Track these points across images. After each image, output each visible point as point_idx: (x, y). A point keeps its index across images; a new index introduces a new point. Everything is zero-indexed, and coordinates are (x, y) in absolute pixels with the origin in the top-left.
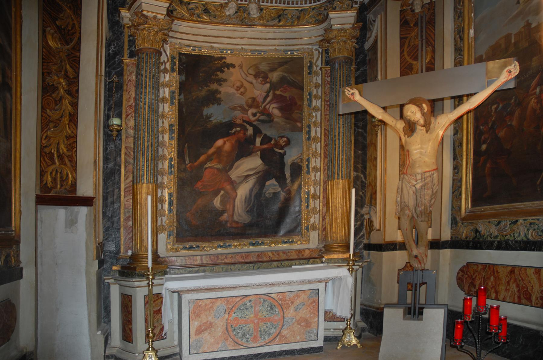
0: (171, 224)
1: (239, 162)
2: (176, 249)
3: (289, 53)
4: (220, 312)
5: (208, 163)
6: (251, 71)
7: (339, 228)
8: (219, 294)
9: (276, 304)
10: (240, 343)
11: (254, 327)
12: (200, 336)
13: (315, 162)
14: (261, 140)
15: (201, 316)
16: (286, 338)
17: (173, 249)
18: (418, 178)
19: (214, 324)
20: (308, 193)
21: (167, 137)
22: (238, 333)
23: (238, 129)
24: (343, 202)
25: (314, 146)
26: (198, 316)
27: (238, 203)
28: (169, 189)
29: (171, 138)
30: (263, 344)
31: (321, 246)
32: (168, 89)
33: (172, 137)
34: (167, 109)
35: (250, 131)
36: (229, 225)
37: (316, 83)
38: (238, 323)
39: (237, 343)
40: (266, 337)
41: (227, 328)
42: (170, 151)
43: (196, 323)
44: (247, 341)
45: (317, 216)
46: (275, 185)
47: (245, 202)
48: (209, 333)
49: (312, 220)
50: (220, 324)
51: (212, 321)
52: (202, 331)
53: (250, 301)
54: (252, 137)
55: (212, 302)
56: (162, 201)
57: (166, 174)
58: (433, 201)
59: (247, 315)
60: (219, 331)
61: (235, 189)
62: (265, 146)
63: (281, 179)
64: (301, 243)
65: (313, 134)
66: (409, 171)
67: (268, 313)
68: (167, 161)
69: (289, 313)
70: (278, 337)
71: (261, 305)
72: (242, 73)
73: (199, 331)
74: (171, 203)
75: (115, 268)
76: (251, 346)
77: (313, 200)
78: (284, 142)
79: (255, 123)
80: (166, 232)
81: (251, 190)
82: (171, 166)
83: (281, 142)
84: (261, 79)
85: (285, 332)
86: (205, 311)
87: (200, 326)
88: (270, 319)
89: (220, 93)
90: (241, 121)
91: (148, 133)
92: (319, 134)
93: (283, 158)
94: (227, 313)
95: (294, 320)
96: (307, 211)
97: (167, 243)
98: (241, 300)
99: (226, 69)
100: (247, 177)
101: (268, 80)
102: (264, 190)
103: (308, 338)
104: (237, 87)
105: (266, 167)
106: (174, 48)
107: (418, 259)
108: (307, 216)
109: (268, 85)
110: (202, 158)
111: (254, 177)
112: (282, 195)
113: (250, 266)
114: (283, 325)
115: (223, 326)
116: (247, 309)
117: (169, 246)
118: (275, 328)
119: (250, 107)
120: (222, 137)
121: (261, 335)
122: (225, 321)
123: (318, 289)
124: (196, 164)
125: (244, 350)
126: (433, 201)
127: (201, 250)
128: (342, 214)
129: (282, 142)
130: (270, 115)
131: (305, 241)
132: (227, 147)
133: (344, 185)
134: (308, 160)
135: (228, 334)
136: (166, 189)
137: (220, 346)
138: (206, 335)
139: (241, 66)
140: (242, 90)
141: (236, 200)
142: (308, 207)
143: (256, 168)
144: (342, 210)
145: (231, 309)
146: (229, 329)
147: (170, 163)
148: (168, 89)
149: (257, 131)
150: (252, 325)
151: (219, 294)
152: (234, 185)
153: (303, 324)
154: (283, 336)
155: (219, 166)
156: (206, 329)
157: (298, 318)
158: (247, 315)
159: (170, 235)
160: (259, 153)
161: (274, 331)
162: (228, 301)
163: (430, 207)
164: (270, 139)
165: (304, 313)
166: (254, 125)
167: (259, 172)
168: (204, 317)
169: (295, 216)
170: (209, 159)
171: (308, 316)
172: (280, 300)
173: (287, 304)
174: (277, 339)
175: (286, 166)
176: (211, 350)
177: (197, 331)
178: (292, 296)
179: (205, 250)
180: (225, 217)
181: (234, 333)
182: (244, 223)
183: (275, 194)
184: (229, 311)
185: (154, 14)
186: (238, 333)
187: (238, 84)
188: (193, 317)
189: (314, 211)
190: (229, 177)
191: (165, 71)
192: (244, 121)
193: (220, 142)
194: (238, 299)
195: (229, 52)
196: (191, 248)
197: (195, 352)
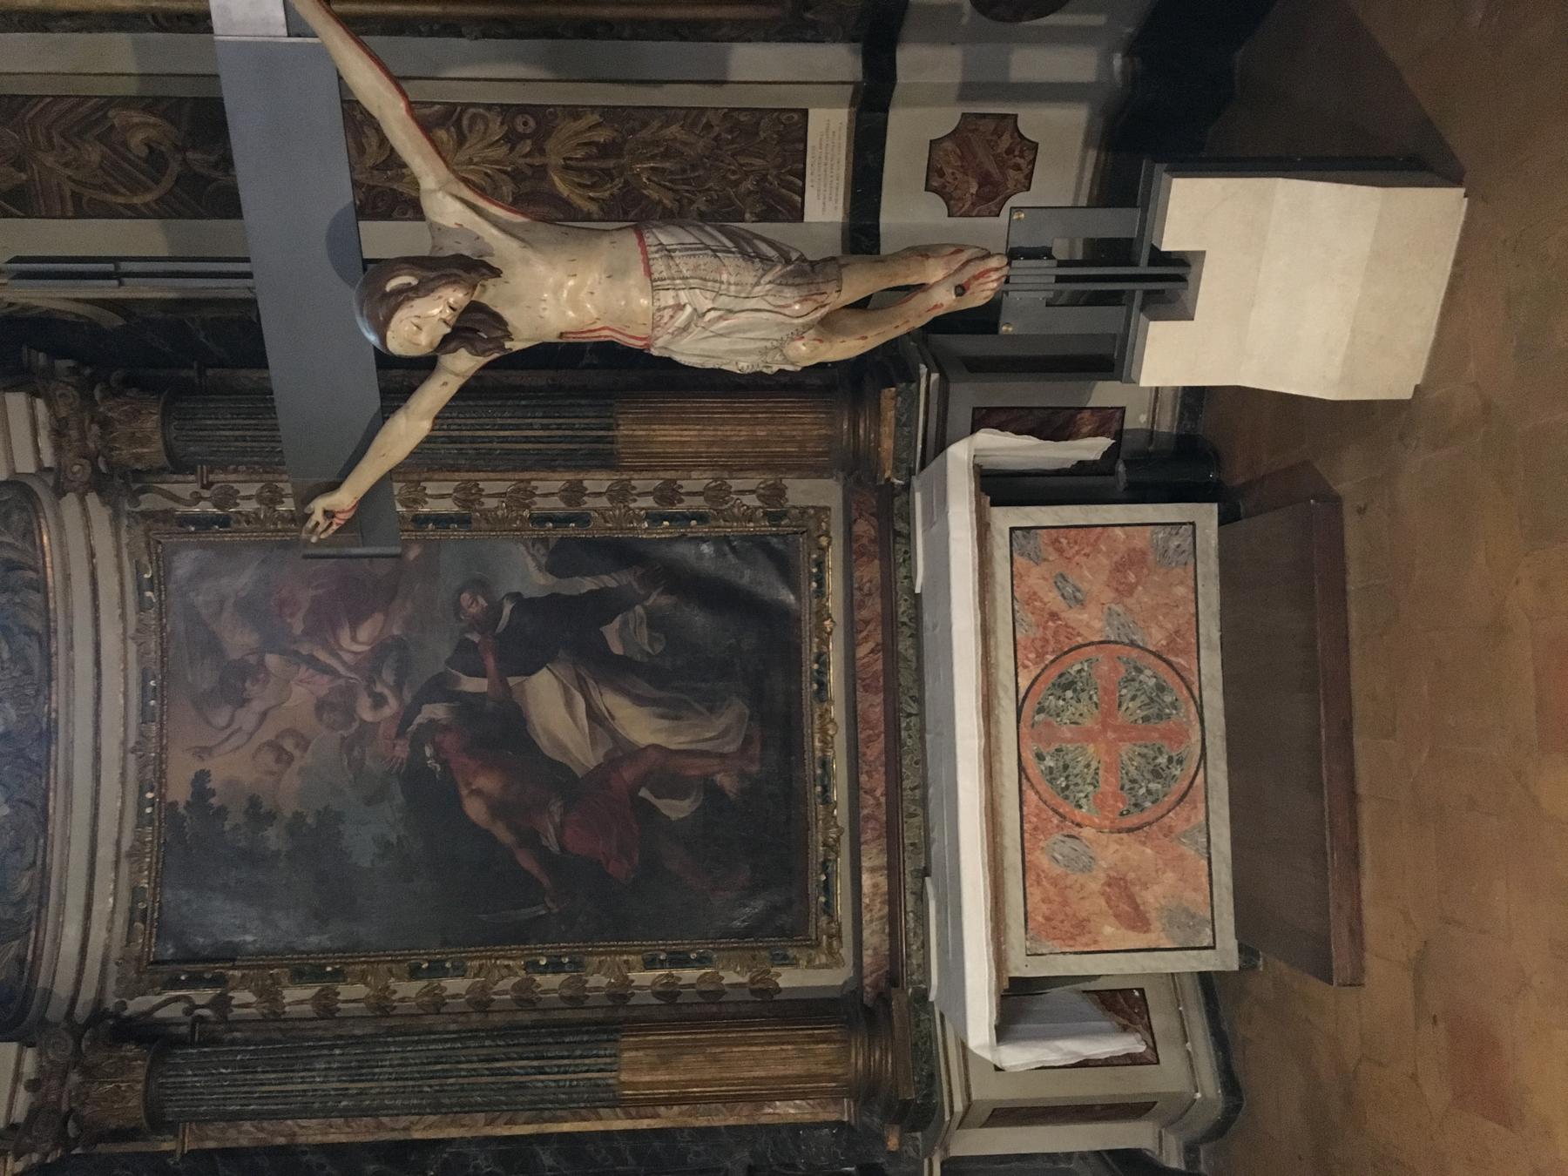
0: (748, 955)
1: (544, 743)
2: (830, 937)
3: (149, 594)
4: (1073, 855)
5: (544, 842)
6: (221, 718)
7: (787, 430)
8: (1012, 857)
9: (1053, 673)
10: (1186, 784)
11: (1130, 740)
12: (1152, 915)
13: (546, 495)
14: (470, 675)
15: (1084, 914)
16: (1177, 632)
17: (830, 945)
18: (671, 302)
19: (1113, 874)
20: (655, 518)
21: (455, 986)
22: (1149, 792)
23: (428, 751)
24: (698, 421)
25: (491, 503)
26: (1082, 925)
27: (682, 739)
28: (630, 970)
29: (460, 971)
30: (1193, 709)
31: (841, 475)
32: (285, 992)
33: (455, 968)
34: (360, 990)
35: (437, 711)
36: (755, 768)
37: (259, 498)
38: (1114, 793)
39: (1185, 794)
40: (1168, 699)
41: (1130, 830)
42: (504, 972)
43: (1108, 930)
44: (1180, 762)
45: (735, 484)
46: (625, 623)
47: (677, 718)
48: (1145, 886)
49: (751, 501)
50: (1112, 852)
51: (1102, 877)
52: (1136, 907)
53: (1040, 757)
54: (457, 704)
55: (1039, 883)
56: (669, 993)
57: (579, 979)
58: (764, 247)
59: (1088, 766)
60: (1136, 854)
61: (634, 753)
62: (490, 663)
63: (604, 606)
64: (827, 534)
65: (447, 507)
66: (642, 331)
67: (1084, 696)
68: (538, 978)
69: (1088, 626)
70: (1172, 659)
71: (1054, 721)
72: (227, 747)
73: (1137, 919)
74: (680, 960)
75: (893, 1143)
76: (1198, 751)
77: (681, 501)
78: (475, 600)
79: (408, 697)
80: (773, 970)
81: (639, 700)
82: (555, 967)
83: (474, 610)
84: (248, 684)
85: (1156, 638)
86: (1065, 903)
87: (1117, 916)
88: (1105, 689)
89: (298, 816)
90: (401, 742)
91: (446, 1074)
92: (448, 488)
93: (532, 600)
94: (1076, 831)
95: (1118, 609)
96: (716, 519)
97: (810, 964)
98: (1032, 786)
99: (212, 800)
100: (593, 715)
101: (252, 659)
102: (638, 657)
103: (1182, 559)
104: (278, 760)
105: (561, 654)
106: (139, 981)
107: (969, 282)
108: (737, 520)
109: (272, 660)
110: (526, 861)
111: (595, 694)
112: (659, 600)
113: (908, 728)
114: (1132, 644)
115: (1120, 842)
116: (1066, 767)
117: (823, 959)
118: (1139, 671)
119: (350, 713)
120: (457, 800)
121: (1159, 717)
122: (1104, 837)
123: (1012, 530)
124: (545, 881)
125: (1210, 771)
126: (764, 247)
127: (837, 854)
128: (741, 422)
129: (474, 606)
130: (381, 650)
131: (820, 521)
132: (488, 782)
133: (637, 421)
134: (540, 520)
135: (1149, 824)
136: (632, 975)
137: (1189, 851)
138: (1151, 898)
139: (203, 752)
140: (288, 745)
141: (673, 747)
142: (702, 518)
143: (566, 690)
144: (724, 422)
145: (1063, 817)
146: (1133, 821)
147: (544, 970)
148: (285, 992)
149: (439, 689)
150: (1125, 748)
151: (1012, 857)
152: (622, 753)
153: (1132, 578)
154: (1171, 641)
155: (556, 807)
156: (1131, 899)
157: (1109, 595)
158: (1088, 766)
159: (785, 957)
160: (512, 681)
161: (1148, 672)
162: (1036, 829)
163: (788, 261)
164: (464, 647)
165: (1093, 576)
166: (415, 698)
167: (579, 677)
168: (1087, 903)
169: (730, 556)
170: (531, 840)
171: (1105, 561)
172: (1040, 656)
173: (1056, 633)
174: (1180, 661)
175: (557, 590)
176: (1205, 880)
177: (1133, 928)
178: (1031, 618)
179: (837, 840)
180: (726, 781)
181: (1148, 804)
182: (751, 718)
183: (655, 622)
184: (1071, 827)
185: (21, 1088)
186: (1149, 792)
187: (268, 758)
188: (1084, 940)
189: (717, 494)
190: (591, 774)
191: (221, 1004)
192: (400, 734)
193: (475, 809)
194: (1031, 796)
195: (150, 795)
196: (827, 888)
197: (1209, 932)
